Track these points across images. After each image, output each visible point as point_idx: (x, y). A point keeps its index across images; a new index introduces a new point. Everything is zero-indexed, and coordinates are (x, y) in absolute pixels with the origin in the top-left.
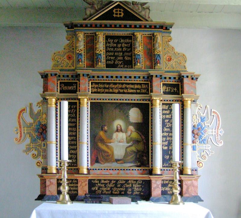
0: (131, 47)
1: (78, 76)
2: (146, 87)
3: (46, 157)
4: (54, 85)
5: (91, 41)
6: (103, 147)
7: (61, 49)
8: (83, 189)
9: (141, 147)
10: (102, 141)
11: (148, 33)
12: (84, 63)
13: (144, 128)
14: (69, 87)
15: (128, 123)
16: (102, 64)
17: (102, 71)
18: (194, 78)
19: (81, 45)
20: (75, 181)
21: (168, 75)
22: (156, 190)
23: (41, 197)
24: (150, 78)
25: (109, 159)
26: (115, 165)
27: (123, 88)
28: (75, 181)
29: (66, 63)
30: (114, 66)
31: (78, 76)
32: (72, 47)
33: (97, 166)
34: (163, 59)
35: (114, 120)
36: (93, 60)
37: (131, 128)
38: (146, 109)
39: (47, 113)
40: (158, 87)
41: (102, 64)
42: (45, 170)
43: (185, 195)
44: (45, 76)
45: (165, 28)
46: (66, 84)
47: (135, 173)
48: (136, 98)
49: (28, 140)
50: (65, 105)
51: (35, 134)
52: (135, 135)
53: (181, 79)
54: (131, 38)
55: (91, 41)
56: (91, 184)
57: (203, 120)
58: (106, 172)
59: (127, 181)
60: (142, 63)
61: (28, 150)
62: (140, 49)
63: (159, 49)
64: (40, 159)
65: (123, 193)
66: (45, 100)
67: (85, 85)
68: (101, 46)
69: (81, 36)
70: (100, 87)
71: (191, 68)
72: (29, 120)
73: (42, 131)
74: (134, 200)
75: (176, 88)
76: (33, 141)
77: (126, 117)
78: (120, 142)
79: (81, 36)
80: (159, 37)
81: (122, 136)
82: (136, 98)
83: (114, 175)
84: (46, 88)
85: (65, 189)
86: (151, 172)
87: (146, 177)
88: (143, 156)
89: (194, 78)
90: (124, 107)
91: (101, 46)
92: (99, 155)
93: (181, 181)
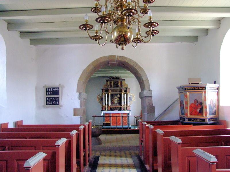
0: (118, 84)
1: (108, 89)
2: (120, 91)
3: (102, 103)
4: (104, 91)
5: (110, 83)
6: (113, 102)
7: (105, 84)
8: (109, 109)
9: (120, 101)
10: (113, 100)
11: (121, 81)
12: (109, 87)
13: (120, 98)
14: (107, 92)
15: (117, 97)
16: (112, 87)
17: (113, 88)
18: (129, 89)
19: (109, 84)
20: (204, 88)
21: (124, 88)
22: (122, 109)
23: (102, 111)
24: (121, 89)
25: (117, 11)
26: (115, 105)
27: (116, 91)
28: (204, 88)
29: (106, 87)
30: (115, 87)
31: (108, 89)
32: (107, 84)
33: (112, 105)
34: (124, 85)
35: (115, 96)
36: (111, 86)
37: (118, 98)
38: (120, 95)
39: (103, 96)
40: (123, 91)
41: (112, 87)
42: (102, 106)
43: (128, 110)
44: (102, 89)
45: (124, 80)
46: (106, 91)
47: (118, 106)
48: (119, 93)
49: (99, 101)
50: (106, 95)
51: (100, 100)
52: (118, 99)
53: (127, 89)
54: (118, 82)
55: (110, 83)
56: (111, 108)
57: (131, 96)
58: (113, 106)
59: (117, 108)
60: (120, 86)
61: (99, 102)
62: (119, 84)
63: (123, 84)
64: (101, 104)
65: (117, 110)
66: (102, 94)
67: (110, 91)
68: (112, 84)
69: (109, 82)
70: (112, 91)
71: (129, 87)
72: (99, 97)
73: (102, 99)
74: (118, 110)
75: (126, 91)
76: (100, 101)
77: (117, 96)
78: (116, 101)
79: (109, 82)
80: (123, 82)
81: (116, 99)
82: (119, 93)
83: (115, 107)
84: (102, 92)
85: (107, 109)
86: (121, 106)
87: (120, 107)
88: (120, 103)
89: (129, 89)
90: (116, 95)
91: (112, 84)
92: (112, 103)
93: (127, 108)
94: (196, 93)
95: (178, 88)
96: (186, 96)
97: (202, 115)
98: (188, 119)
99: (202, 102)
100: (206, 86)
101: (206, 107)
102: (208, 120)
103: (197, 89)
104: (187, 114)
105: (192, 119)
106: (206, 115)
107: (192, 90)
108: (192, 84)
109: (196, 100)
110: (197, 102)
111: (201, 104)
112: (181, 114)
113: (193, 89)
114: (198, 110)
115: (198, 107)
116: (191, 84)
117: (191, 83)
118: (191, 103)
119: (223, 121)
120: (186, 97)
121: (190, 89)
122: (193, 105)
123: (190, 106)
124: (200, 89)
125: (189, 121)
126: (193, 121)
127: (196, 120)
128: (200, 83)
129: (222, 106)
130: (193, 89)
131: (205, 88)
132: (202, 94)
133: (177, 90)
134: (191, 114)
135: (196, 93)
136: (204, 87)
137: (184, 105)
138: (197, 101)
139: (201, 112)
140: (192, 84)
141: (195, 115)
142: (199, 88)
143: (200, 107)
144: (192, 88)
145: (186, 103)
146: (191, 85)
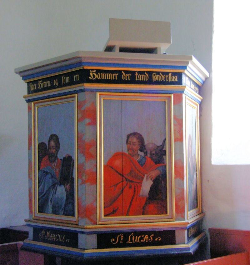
20: (175, 79)
94: (133, 97)
95: (24, 78)
96: (90, 115)
97: (163, 210)
98: (95, 236)
99: (164, 145)
100: (185, 68)
101: (180, 173)
102: (93, 240)
103: (141, 78)
104: (89, 212)
105: (114, 234)
106: (180, 211)
107: (119, 81)
108: (123, 50)
109: (134, 134)
110: (142, 147)
111: (159, 155)
112: (42, 209)
113: (125, 76)
114: (146, 186)
115: (146, 169)
116: (117, 50)
117: (118, 44)
118: (113, 152)
119: (230, 231)
120: (88, 121)
121: (110, 76)
122: (118, 163)
123: (109, 167)
124: (157, 83)
125: (99, 247)
126: (119, 245)
127: (137, 239)
128: (163, 48)
129: (228, 170)
130: (125, 76)
131: (180, 75)
132: (164, 108)
133: (22, 87)
134: (110, 211)
135: (139, 98)
136: (174, 74)
137: (68, 161)
138: (140, 138)
139: (158, 197)
140: (123, 50)
141: (127, 215)
142: (150, 73)
143: (155, 173)
144: (120, 72)
145: (89, 150)
146: (116, 55)
